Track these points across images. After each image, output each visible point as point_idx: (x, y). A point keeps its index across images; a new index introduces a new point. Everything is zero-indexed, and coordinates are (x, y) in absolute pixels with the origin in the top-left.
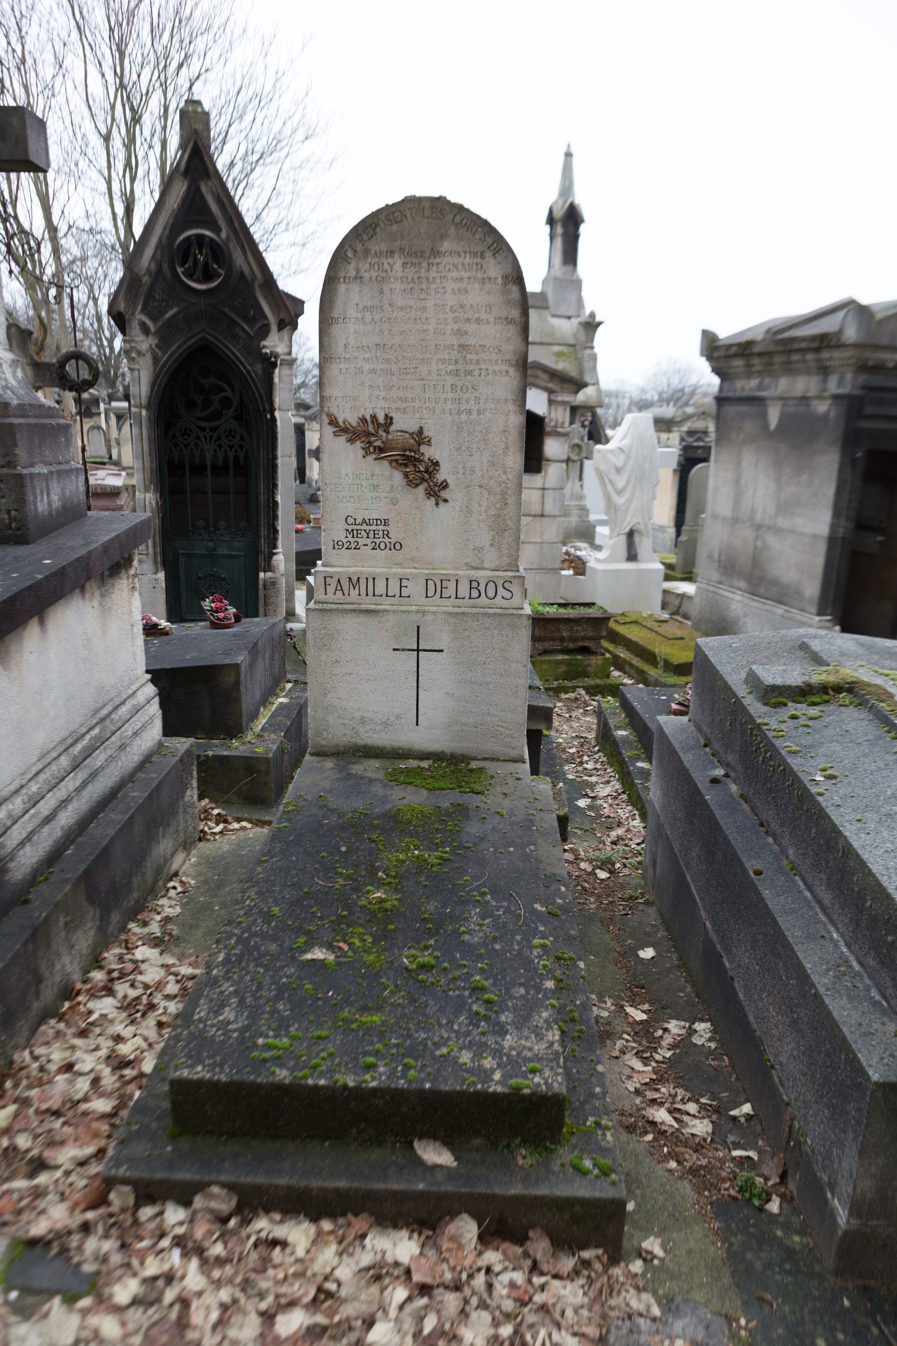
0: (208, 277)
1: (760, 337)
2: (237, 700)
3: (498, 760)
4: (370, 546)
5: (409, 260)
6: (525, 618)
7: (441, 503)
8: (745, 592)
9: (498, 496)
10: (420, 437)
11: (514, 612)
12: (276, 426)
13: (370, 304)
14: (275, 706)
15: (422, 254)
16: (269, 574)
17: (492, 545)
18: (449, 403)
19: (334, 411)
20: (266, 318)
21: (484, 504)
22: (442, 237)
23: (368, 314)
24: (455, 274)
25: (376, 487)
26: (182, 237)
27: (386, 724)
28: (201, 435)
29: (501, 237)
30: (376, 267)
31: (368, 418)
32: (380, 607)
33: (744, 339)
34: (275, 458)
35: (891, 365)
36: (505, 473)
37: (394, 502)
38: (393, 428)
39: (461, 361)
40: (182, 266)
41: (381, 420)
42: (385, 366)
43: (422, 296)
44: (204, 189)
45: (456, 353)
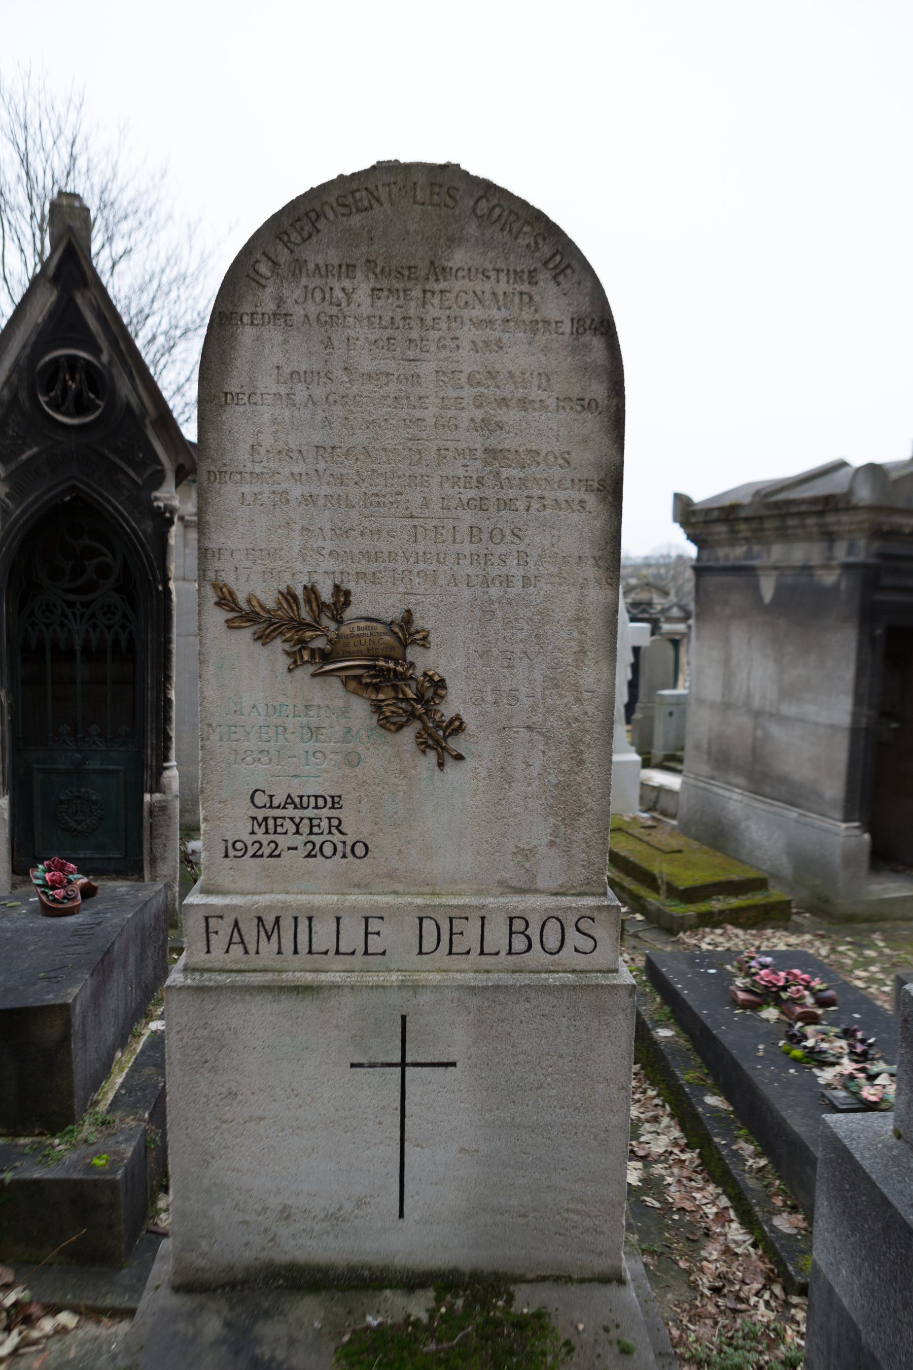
0: (81, 408)
1: (746, 500)
2: (66, 1066)
3: (569, 1279)
4: (303, 851)
5: (385, 283)
6: (624, 993)
7: (449, 763)
8: (745, 790)
9: (565, 748)
10: (406, 632)
11: (602, 980)
12: (170, 600)
13: (304, 367)
14: (144, 1038)
15: (411, 273)
16: (157, 796)
17: (552, 844)
18: (465, 562)
19: (229, 578)
20: (159, 463)
21: (537, 762)
22: (451, 240)
23: (300, 387)
24: (478, 313)
25: (314, 731)
26: (47, 359)
27: (334, 1218)
28: (69, 612)
29: (570, 243)
30: (318, 295)
31: (299, 592)
32: (323, 977)
33: (726, 502)
34: (168, 641)
35: (907, 530)
36: (578, 700)
37: (352, 760)
38: (350, 613)
39: (489, 481)
40: (46, 394)
41: (326, 595)
42: (336, 490)
43: (411, 354)
44: (79, 300)
45: (479, 464)
